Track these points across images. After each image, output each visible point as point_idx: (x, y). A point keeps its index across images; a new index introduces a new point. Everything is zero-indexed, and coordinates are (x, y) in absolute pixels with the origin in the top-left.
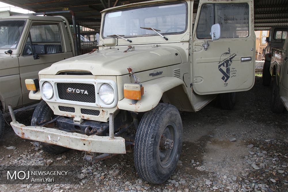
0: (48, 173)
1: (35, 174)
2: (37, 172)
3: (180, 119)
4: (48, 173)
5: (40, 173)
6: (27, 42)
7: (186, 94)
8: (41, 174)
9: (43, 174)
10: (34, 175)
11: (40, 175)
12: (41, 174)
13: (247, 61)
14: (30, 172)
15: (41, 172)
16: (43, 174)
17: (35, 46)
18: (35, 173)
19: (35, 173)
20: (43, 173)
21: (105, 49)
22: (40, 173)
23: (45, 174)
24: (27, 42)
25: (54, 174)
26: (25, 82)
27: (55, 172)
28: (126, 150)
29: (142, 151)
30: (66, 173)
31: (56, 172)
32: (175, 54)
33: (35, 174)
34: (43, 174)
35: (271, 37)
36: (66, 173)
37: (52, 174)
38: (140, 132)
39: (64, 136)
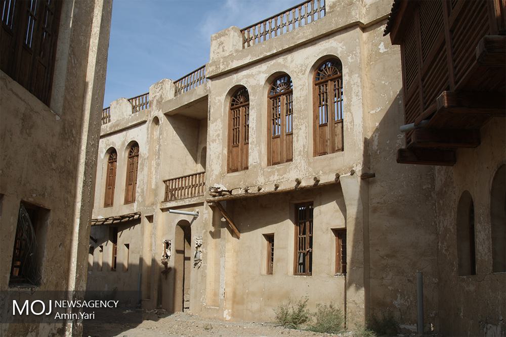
0: (85, 304)
2: (65, 302)
3: (296, 42)
4: (85, 304)
8: (72, 306)
9: (76, 304)
12: (72, 306)
13: (344, 299)
15: (72, 302)
16: (76, 304)
17: (336, 149)
21: (66, 217)
23: (79, 302)
25: (95, 305)
27: (97, 302)
28: (175, 263)
30: (116, 304)
31: (99, 302)
32: (47, 204)
34: (75, 306)
35: (227, 219)
36: (116, 304)
37: (92, 305)
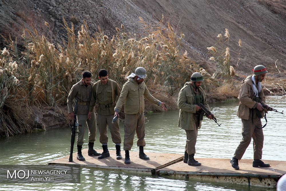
0: (48, 172)
1: (35, 173)
2: (36, 171)
4: (48, 172)
5: (39, 172)
6: (248, 93)
7: (75, 135)
8: (41, 173)
10: (34, 174)
11: (39, 174)
12: (41, 173)
14: (29, 171)
18: (35, 172)
19: (35, 172)
20: (43, 172)
22: (39, 172)
23: (44, 171)
24: (248, 93)
26: (111, 136)
29: (196, 61)
33: (35, 173)
34: (43, 173)
38: (158, 98)
39: (182, 116)
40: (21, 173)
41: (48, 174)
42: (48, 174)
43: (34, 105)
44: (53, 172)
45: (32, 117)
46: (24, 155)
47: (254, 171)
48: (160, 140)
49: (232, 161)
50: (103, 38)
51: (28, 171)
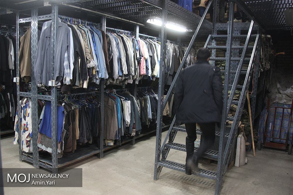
0: (49, 176)
2: (37, 175)
4: (49, 176)
5: (40, 176)
10: (35, 177)
20: (44, 175)
22: (40, 176)
23: (46, 177)
27: (56, 175)
30: (67, 176)
34: (44, 177)
36: (67, 176)
40: (22, 177)
41: (49, 177)
42: (49, 177)
43: (29, 76)
44: (55, 175)
45: (246, 164)
46: (248, 81)
47: (111, 150)
48: (49, 51)
49: (71, 88)
50: (227, 57)
51: (29, 174)
